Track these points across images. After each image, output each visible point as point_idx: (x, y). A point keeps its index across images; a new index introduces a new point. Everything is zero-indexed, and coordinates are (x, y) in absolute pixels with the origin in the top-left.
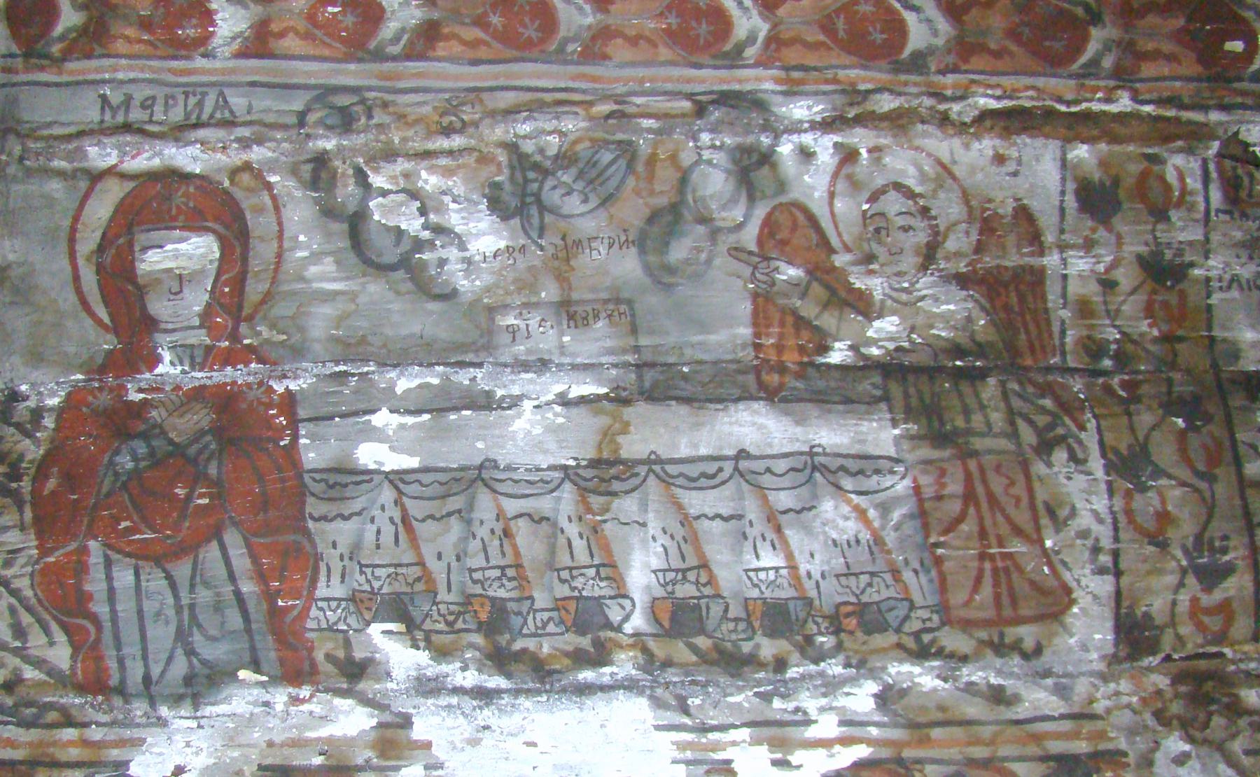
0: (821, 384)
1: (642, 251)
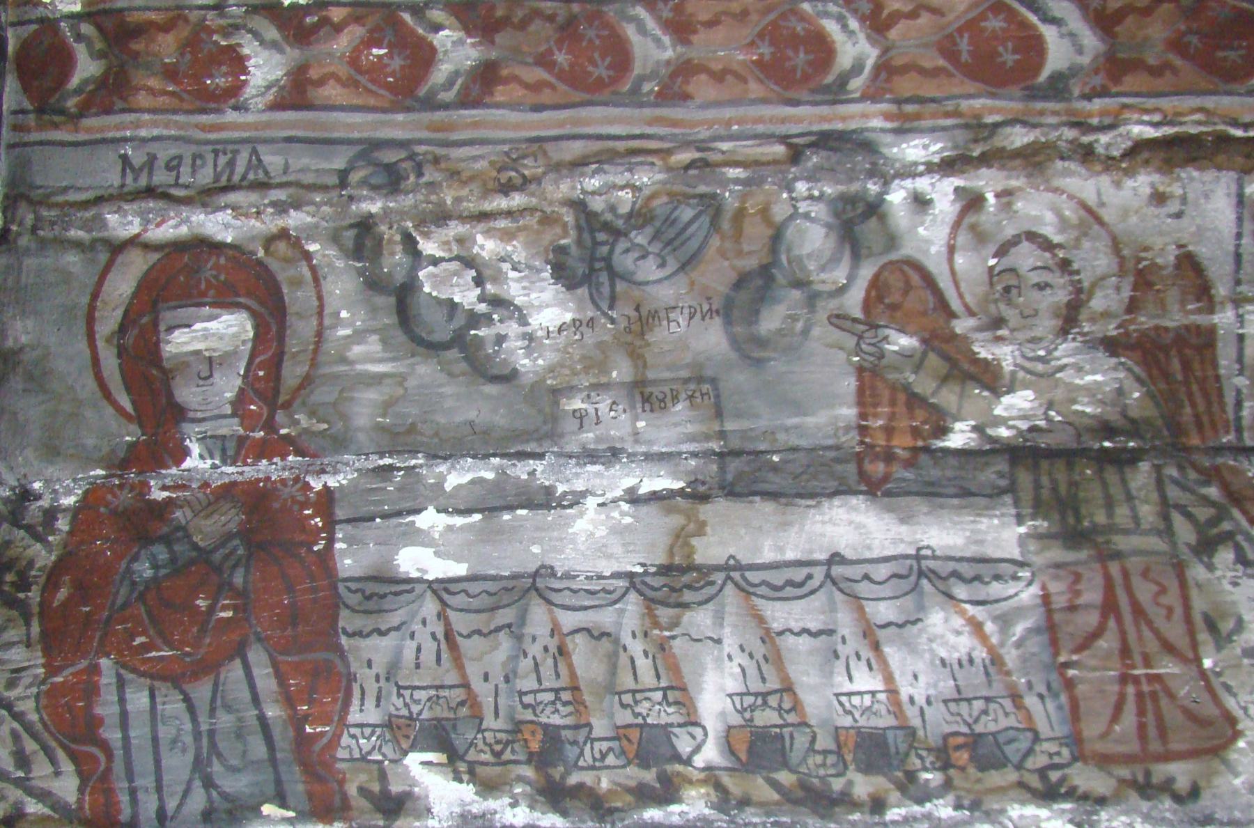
0: (935, 473)
1: (728, 322)
